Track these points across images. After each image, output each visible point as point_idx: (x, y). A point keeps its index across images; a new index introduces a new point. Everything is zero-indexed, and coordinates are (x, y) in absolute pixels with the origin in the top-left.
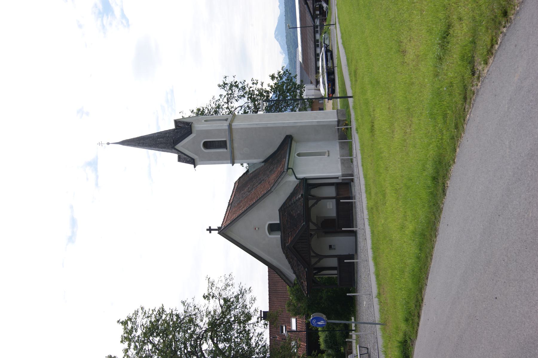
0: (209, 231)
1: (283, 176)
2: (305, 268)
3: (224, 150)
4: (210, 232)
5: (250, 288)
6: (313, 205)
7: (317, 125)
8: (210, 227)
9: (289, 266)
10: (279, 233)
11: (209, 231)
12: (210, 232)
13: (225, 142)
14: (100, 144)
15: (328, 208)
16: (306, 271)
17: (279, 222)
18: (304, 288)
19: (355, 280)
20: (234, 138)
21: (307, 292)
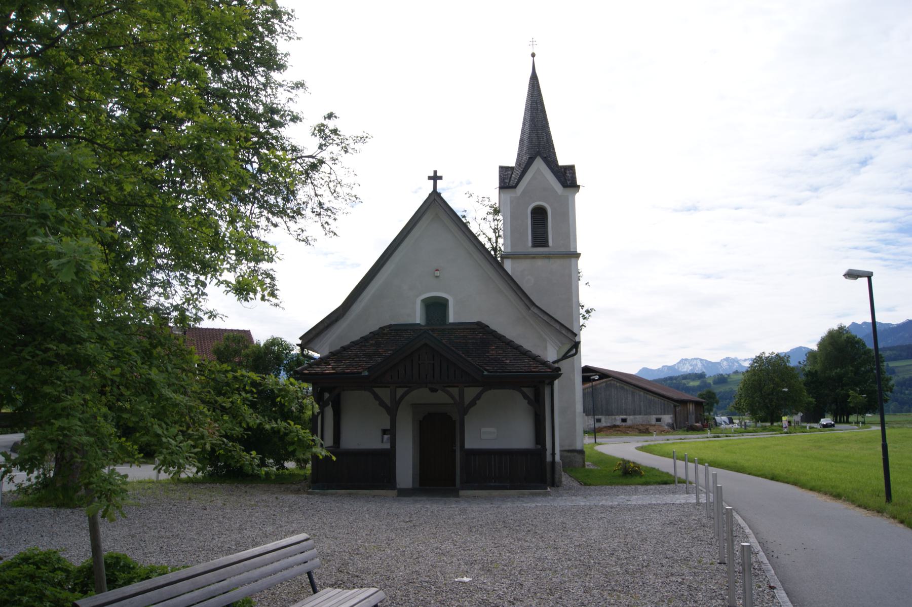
0: (438, 174)
1: (566, 334)
2: (369, 369)
3: (530, 244)
4: (430, 178)
5: (335, 234)
6: (377, 397)
7: (575, 412)
8: (441, 178)
9: (346, 343)
10: (423, 323)
11: (438, 174)
12: (430, 178)
13: (545, 244)
14: (533, 42)
15: (483, 430)
16: (361, 373)
17: (451, 319)
18: (316, 366)
19: (330, 491)
20: (552, 261)
21: (306, 372)
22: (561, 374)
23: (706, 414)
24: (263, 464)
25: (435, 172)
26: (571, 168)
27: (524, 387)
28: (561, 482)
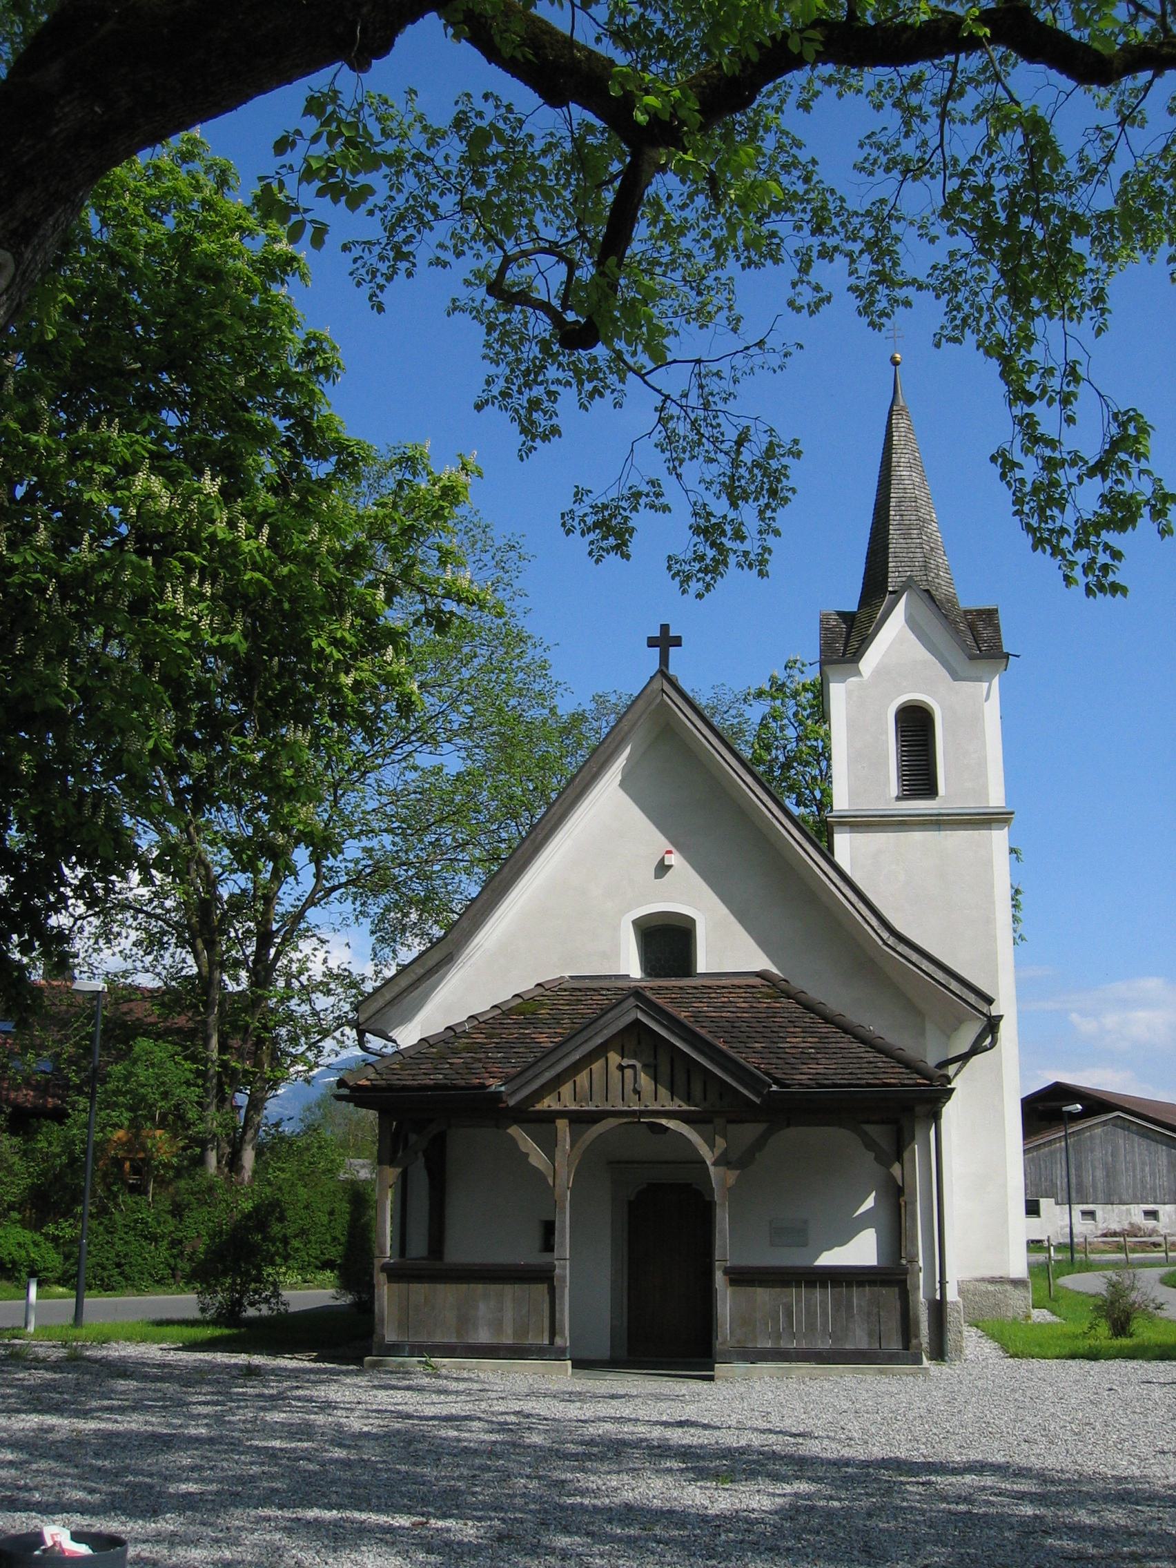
0: (673, 633)
3: (894, 789)
4: (652, 643)
8: (677, 642)
12: (652, 643)
22: (953, 1090)
23: (299, 805)
24: (219, 641)
25: (665, 628)
26: (989, 616)
27: (868, 1122)
28: (960, 1350)
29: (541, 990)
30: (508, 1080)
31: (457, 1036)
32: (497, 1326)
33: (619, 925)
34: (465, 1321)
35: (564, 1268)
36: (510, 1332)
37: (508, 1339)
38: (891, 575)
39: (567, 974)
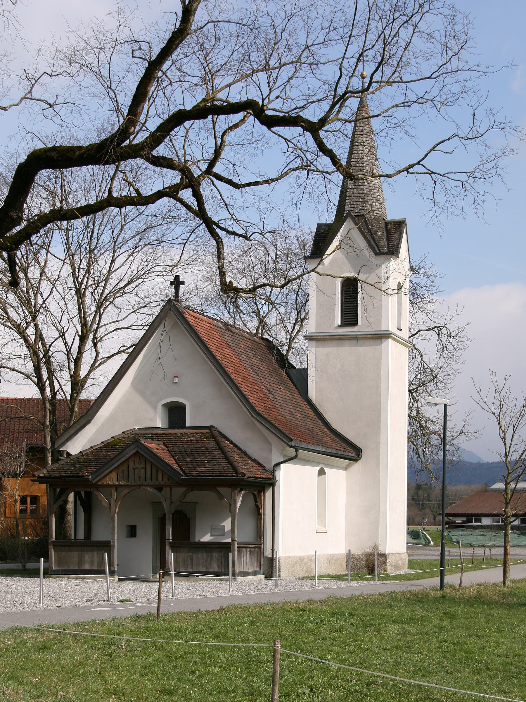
3: (338, 321)
29: (124, 435)
30: (92, 473)
31: (83, 456)
32: (92, 563)
33: (157, 407)
34: (81, 562)
35: (114, 542)
36: (96, 565)
37: (95, 568)
38: (347, 207)
39: (136, 427)
